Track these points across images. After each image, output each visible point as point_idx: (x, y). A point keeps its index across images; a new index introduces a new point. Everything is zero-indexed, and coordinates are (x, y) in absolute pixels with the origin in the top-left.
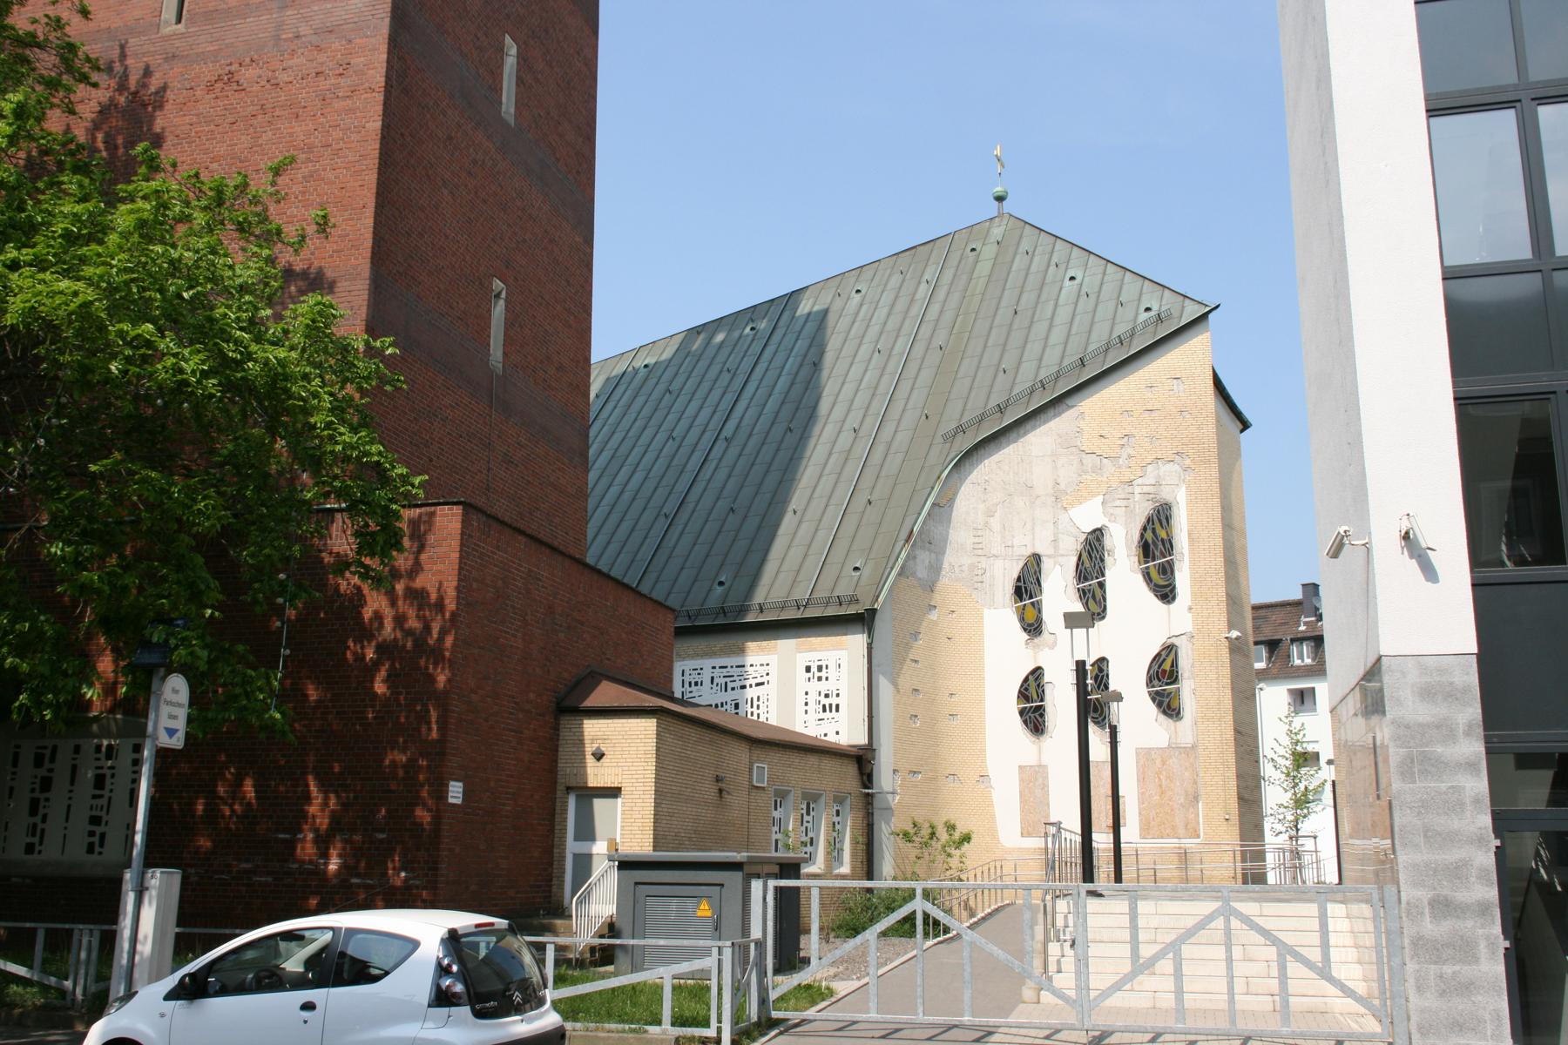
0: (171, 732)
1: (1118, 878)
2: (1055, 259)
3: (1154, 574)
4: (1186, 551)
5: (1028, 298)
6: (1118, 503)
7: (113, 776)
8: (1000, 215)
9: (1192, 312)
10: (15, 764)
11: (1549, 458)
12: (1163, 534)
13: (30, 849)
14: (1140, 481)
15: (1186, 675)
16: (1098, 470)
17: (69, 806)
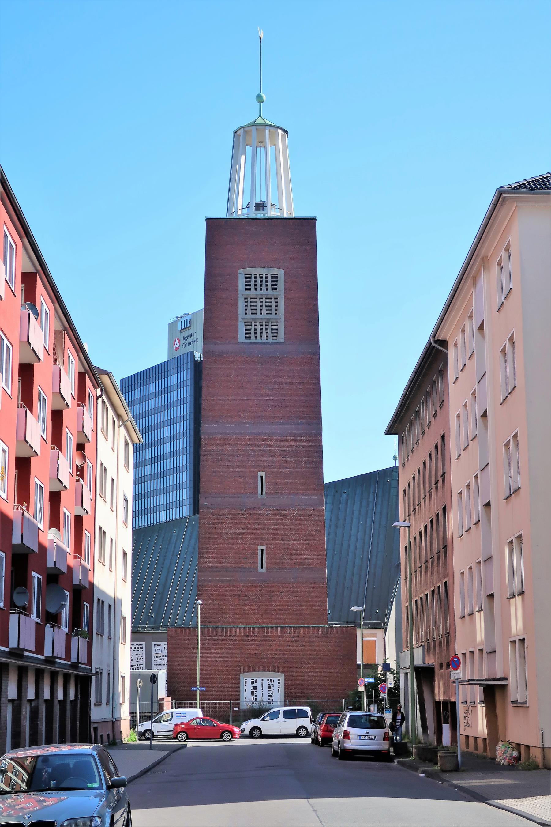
0: (391, 684)
7: (273, 686)
10: (246, 683)
11: (431, 455)
17: (262, 693)
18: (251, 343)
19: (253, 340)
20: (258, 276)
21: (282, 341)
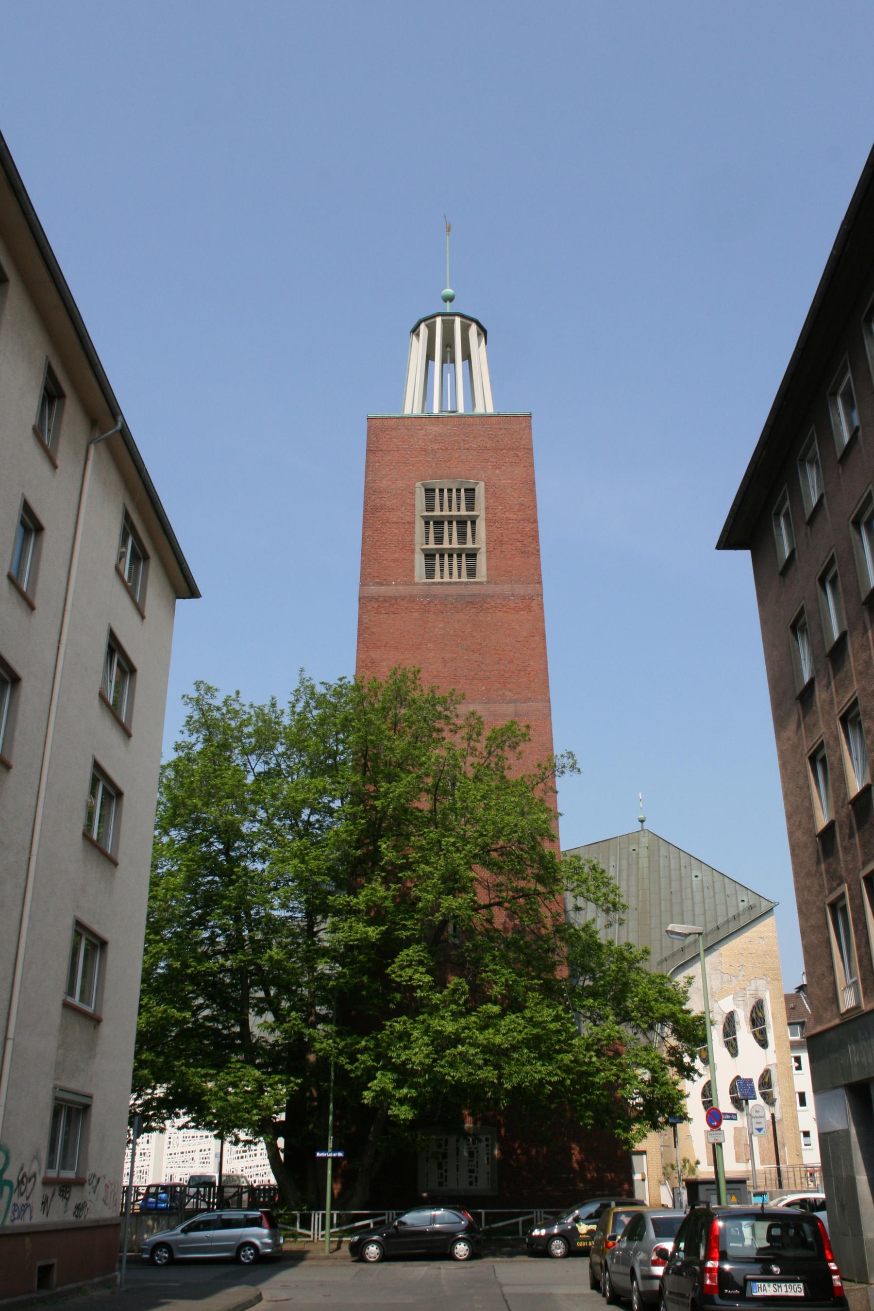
1: (707, 1190)
2: (683, 864)
3: (758, 1034)
4: (771, 1023)
5: (675, 885)
6: (740, 999)
7: (477, 1152)
8: (643, 830)
9: (765, 906)
12: (760, 1015)
13: (441, 1184)
14: (748, 988)
15: (775, 1084)
16: (730, 982)
18: (433, 583)
19: (437, 579)
20: (446, 491)
21: (484, 579)
